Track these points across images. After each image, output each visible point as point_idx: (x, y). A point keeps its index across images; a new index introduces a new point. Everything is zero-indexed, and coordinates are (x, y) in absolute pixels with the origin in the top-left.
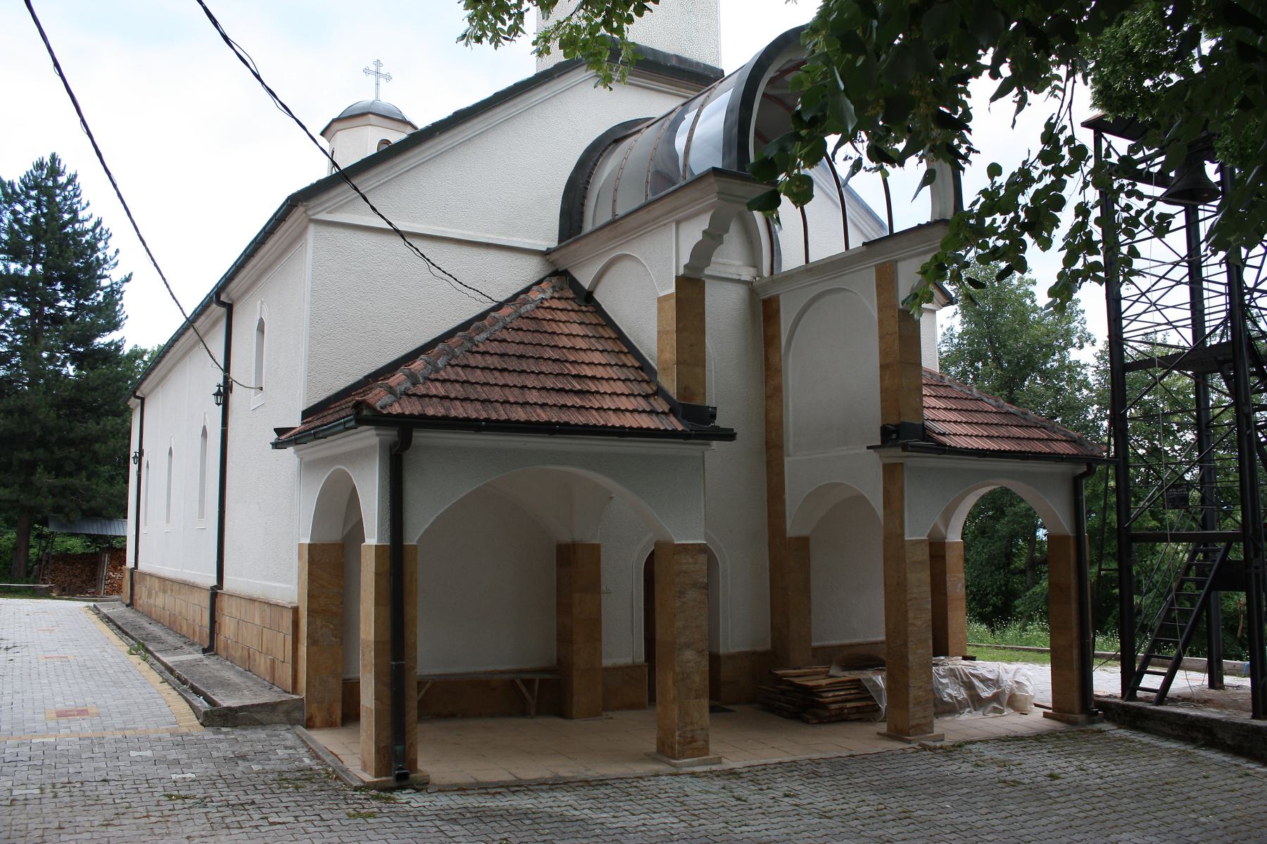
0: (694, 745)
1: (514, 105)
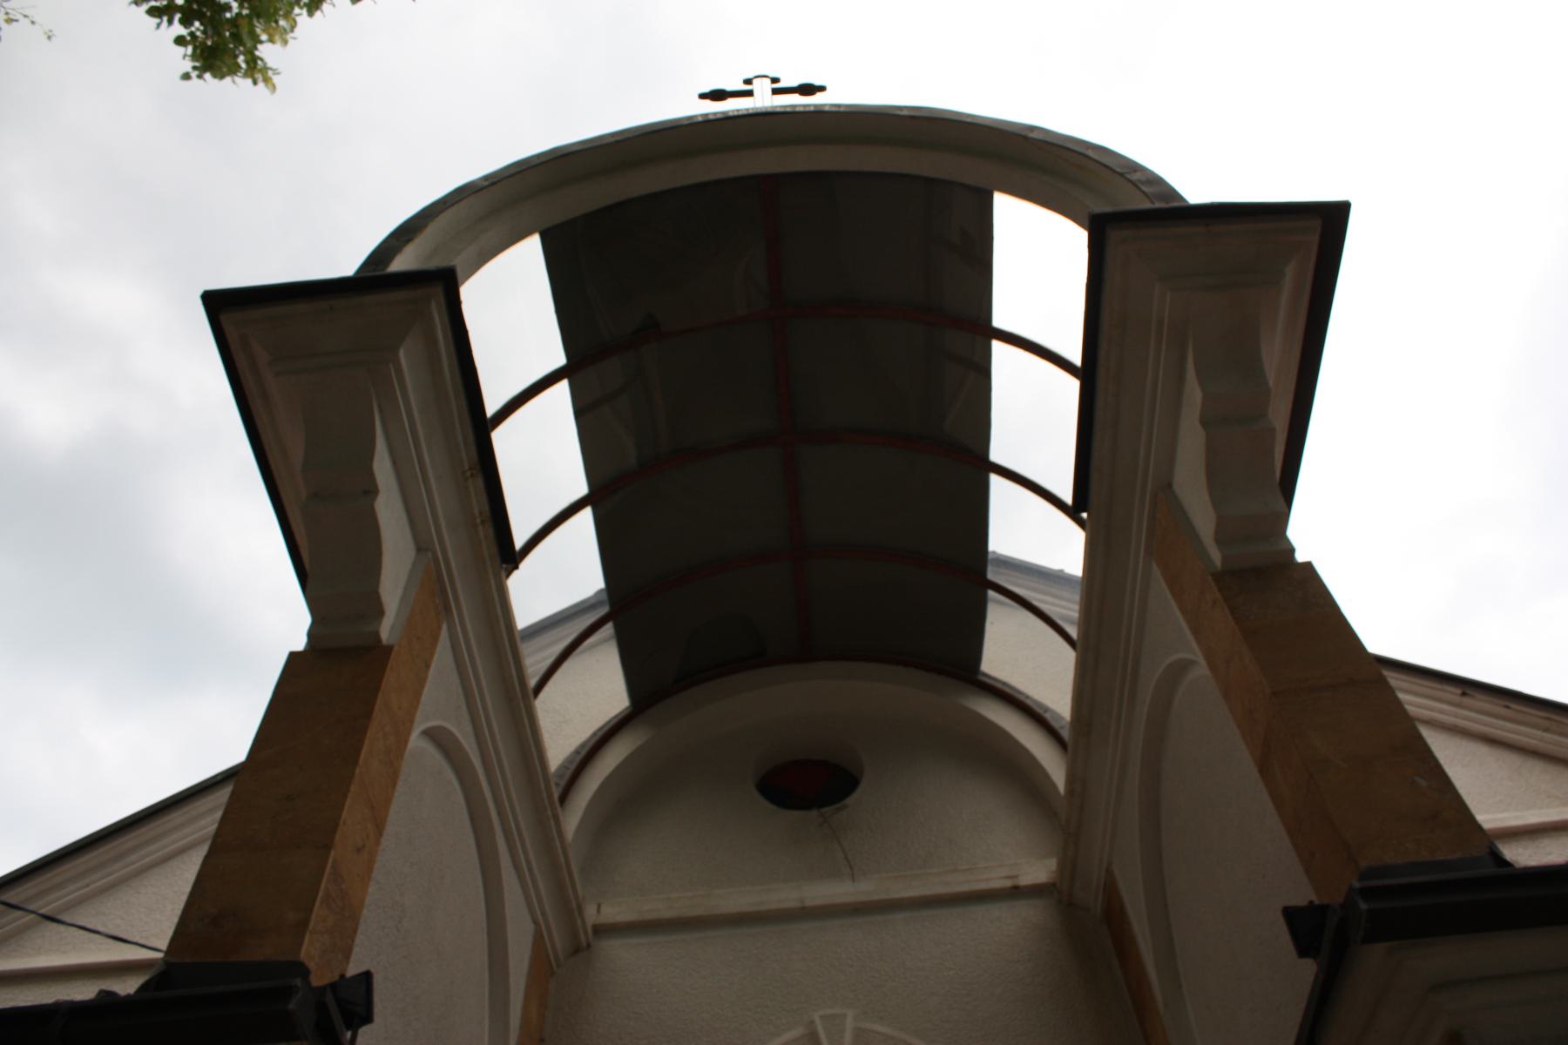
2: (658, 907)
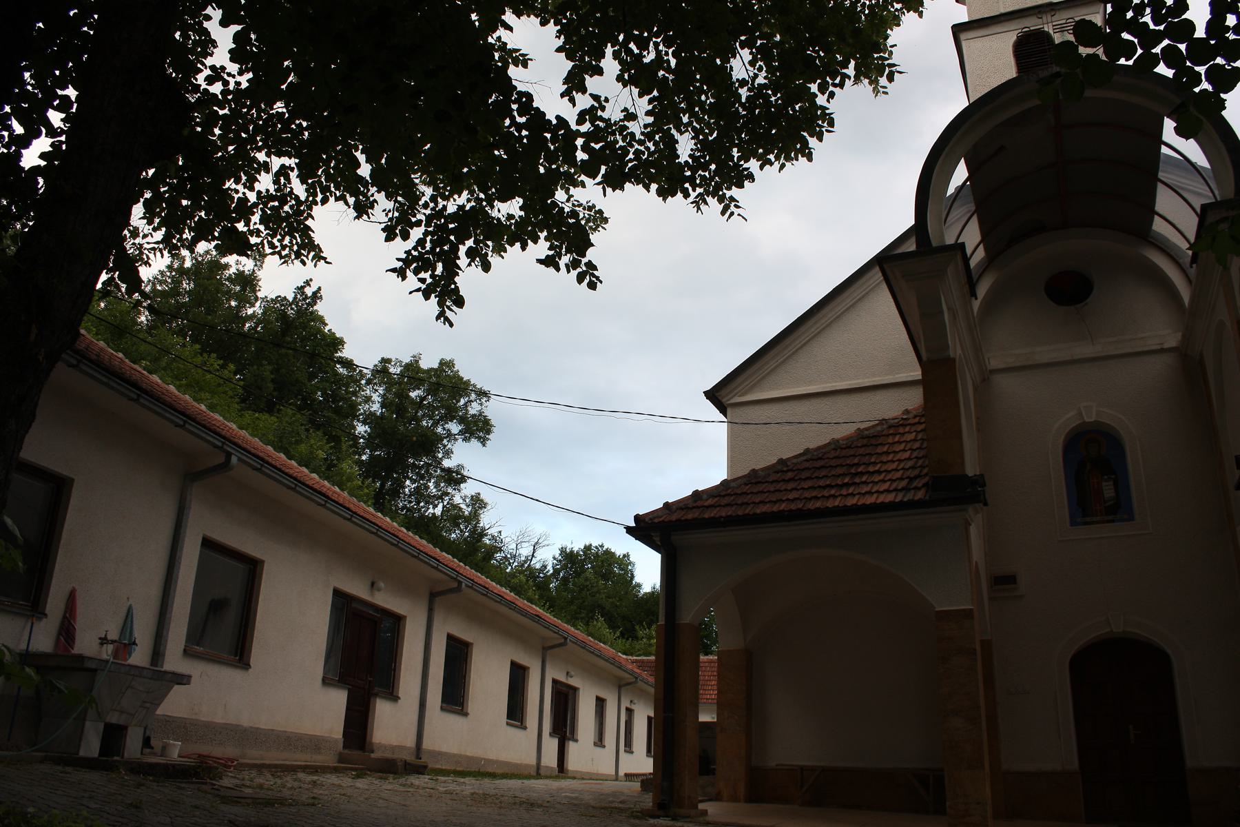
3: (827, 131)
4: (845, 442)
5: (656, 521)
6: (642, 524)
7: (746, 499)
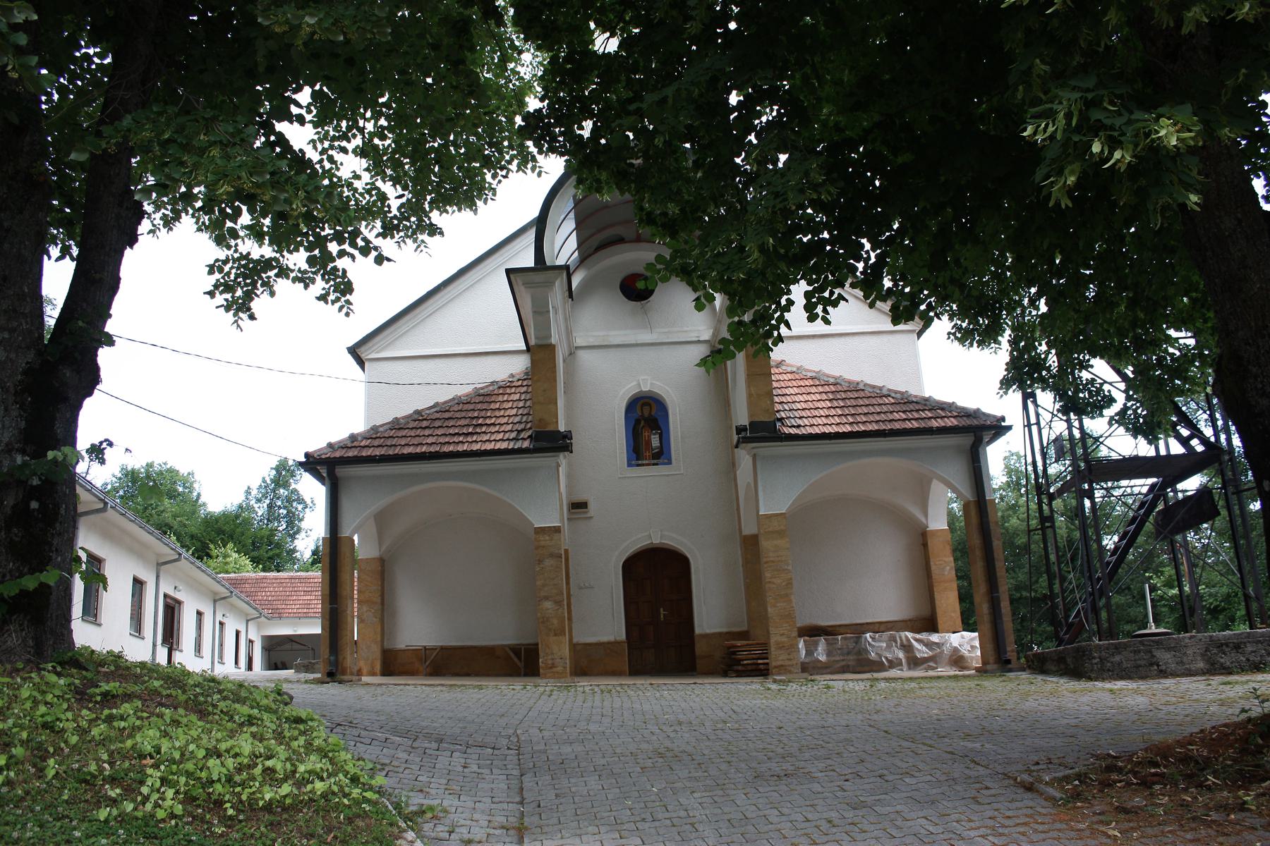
0: (555, 670)
1: (502, 255)
2: (592, 341)
3: (492, 199)
4: (1088, 708)
5: (323, 457)
6: (311, 460)
7: (394, 442)
